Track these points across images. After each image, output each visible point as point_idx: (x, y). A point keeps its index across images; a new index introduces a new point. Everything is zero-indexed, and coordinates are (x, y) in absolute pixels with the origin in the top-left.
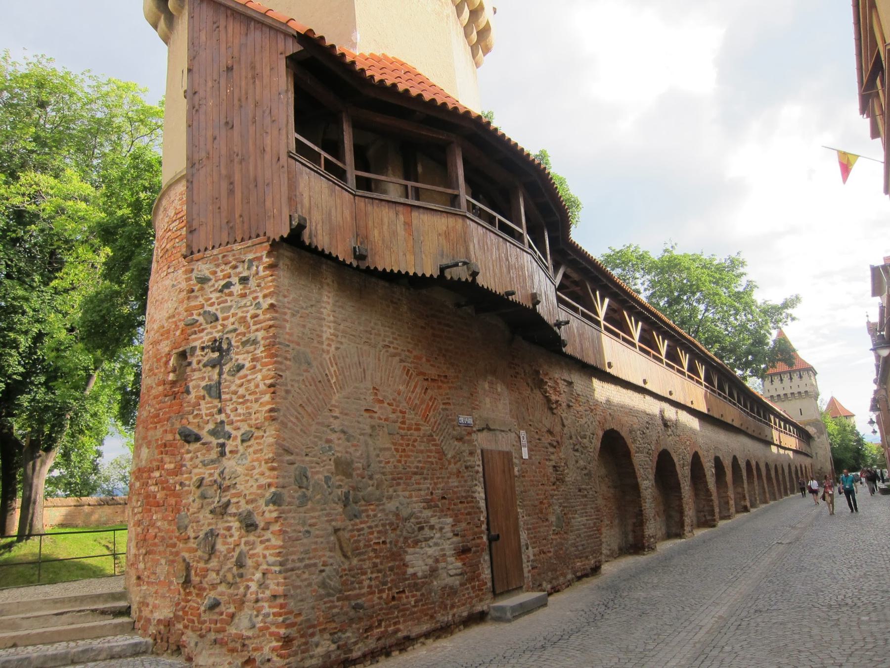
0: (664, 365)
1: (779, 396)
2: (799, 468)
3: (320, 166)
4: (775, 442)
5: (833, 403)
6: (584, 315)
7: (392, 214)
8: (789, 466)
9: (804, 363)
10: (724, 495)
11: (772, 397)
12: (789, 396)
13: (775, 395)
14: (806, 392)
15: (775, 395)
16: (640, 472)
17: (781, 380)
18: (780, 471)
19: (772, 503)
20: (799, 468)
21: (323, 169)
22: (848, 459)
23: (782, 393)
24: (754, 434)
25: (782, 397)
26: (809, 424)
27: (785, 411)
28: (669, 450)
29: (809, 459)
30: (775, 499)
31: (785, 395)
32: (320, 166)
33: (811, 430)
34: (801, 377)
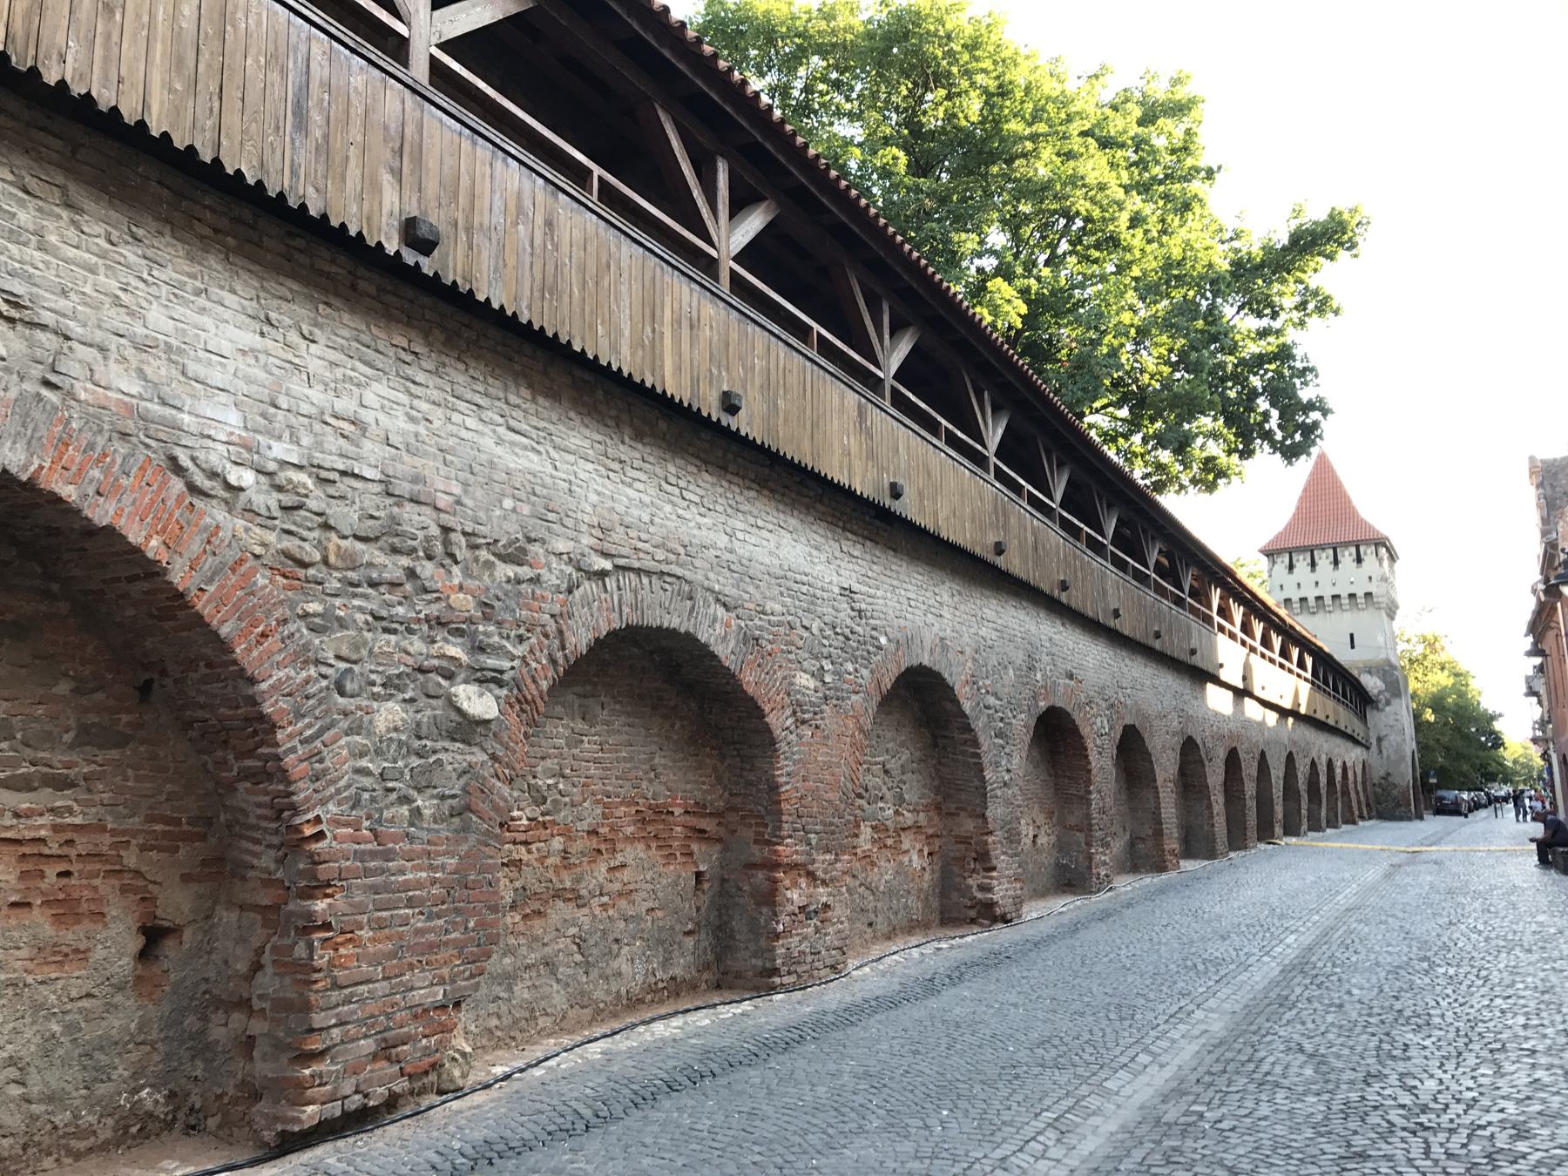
0: (887, 404)
1: (1303, 600)
2: (1322, 769)
4: (1224, 675)
6: (952, 441)
7: (686, 289)
8: (1290, 758)
9: (1363, 524)
10: (758, 853)
11: (1288, 601)
12: (1328, 601)
13: (1295, 598)
14: (1368, 595)
15: (1295, 598)
17: (1313, 564)
20: (1322, 769)
22: (1453, 765)
23: (1311, 594)
25: (1312, 602)
28: (957, 677)
33: (1372, 683)
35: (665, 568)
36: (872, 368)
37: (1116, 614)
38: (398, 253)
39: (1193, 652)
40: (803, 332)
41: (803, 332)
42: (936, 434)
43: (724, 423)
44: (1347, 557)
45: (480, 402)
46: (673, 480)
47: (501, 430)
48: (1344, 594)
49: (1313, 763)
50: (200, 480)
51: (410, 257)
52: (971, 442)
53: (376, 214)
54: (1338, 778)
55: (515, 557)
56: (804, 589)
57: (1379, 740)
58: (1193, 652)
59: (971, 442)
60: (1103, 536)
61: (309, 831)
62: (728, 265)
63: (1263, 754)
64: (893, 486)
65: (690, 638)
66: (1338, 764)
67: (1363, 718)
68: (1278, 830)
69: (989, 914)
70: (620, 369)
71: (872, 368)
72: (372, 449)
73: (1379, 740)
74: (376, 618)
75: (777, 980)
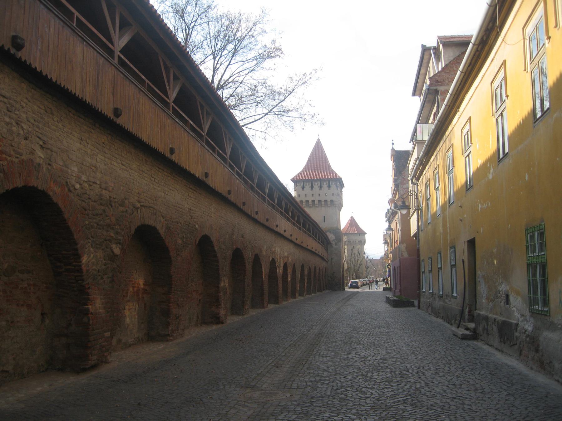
0: (170, 112)
3: (145, 87)
5: (352, 222)
8: (303, 266)
12: (316, 202)
16: (263, 266)
18: (290, 271)
19: (271, 306)
20: (313, 270)
21: (75, 25)
24: (297, 242)
26: (329, 231)
27: (181, 13)
28: (214, 239)
29: (324, 263)
30: (277, 302)
31: (313, 201)
32: (73, 23)
33: (331, 237)
34: (329, 187)
35: (151, 205)
36: (166, 99)
37: (257, 213)
38: (9, 49)
39: (277, 226)
40: (142, 82)
41: (70, 15)
42: (226, 163)
43: (115, 120)
44: (325, 186)
45: (117, 157)
46: (153, 176)
47: (120, 165)
48: (323, 200)
49: (310, 268)
50: (72, 189)
51: (13, 51)
52: (179, 110)
53: (197, 171)
54: (317, 274)
55: (122, 205)
56: (181, 209)
57: (332, 259)
58: (277, 226)
59: (179, 110)
60: (241, 172)
61: (87, 287)
62: (117, 53)
63: (294, 265)
64: (14, 39)
65: (154, 229)
66: (318, 268)
67: (327, 250)
68: (297, 295)
69: (217, 320)
70: (75, 93)
71: (166, 99)
72: (99, 175)
73: (332, 259)
74: (98, 225)
75: (169, 338)
